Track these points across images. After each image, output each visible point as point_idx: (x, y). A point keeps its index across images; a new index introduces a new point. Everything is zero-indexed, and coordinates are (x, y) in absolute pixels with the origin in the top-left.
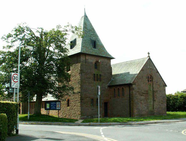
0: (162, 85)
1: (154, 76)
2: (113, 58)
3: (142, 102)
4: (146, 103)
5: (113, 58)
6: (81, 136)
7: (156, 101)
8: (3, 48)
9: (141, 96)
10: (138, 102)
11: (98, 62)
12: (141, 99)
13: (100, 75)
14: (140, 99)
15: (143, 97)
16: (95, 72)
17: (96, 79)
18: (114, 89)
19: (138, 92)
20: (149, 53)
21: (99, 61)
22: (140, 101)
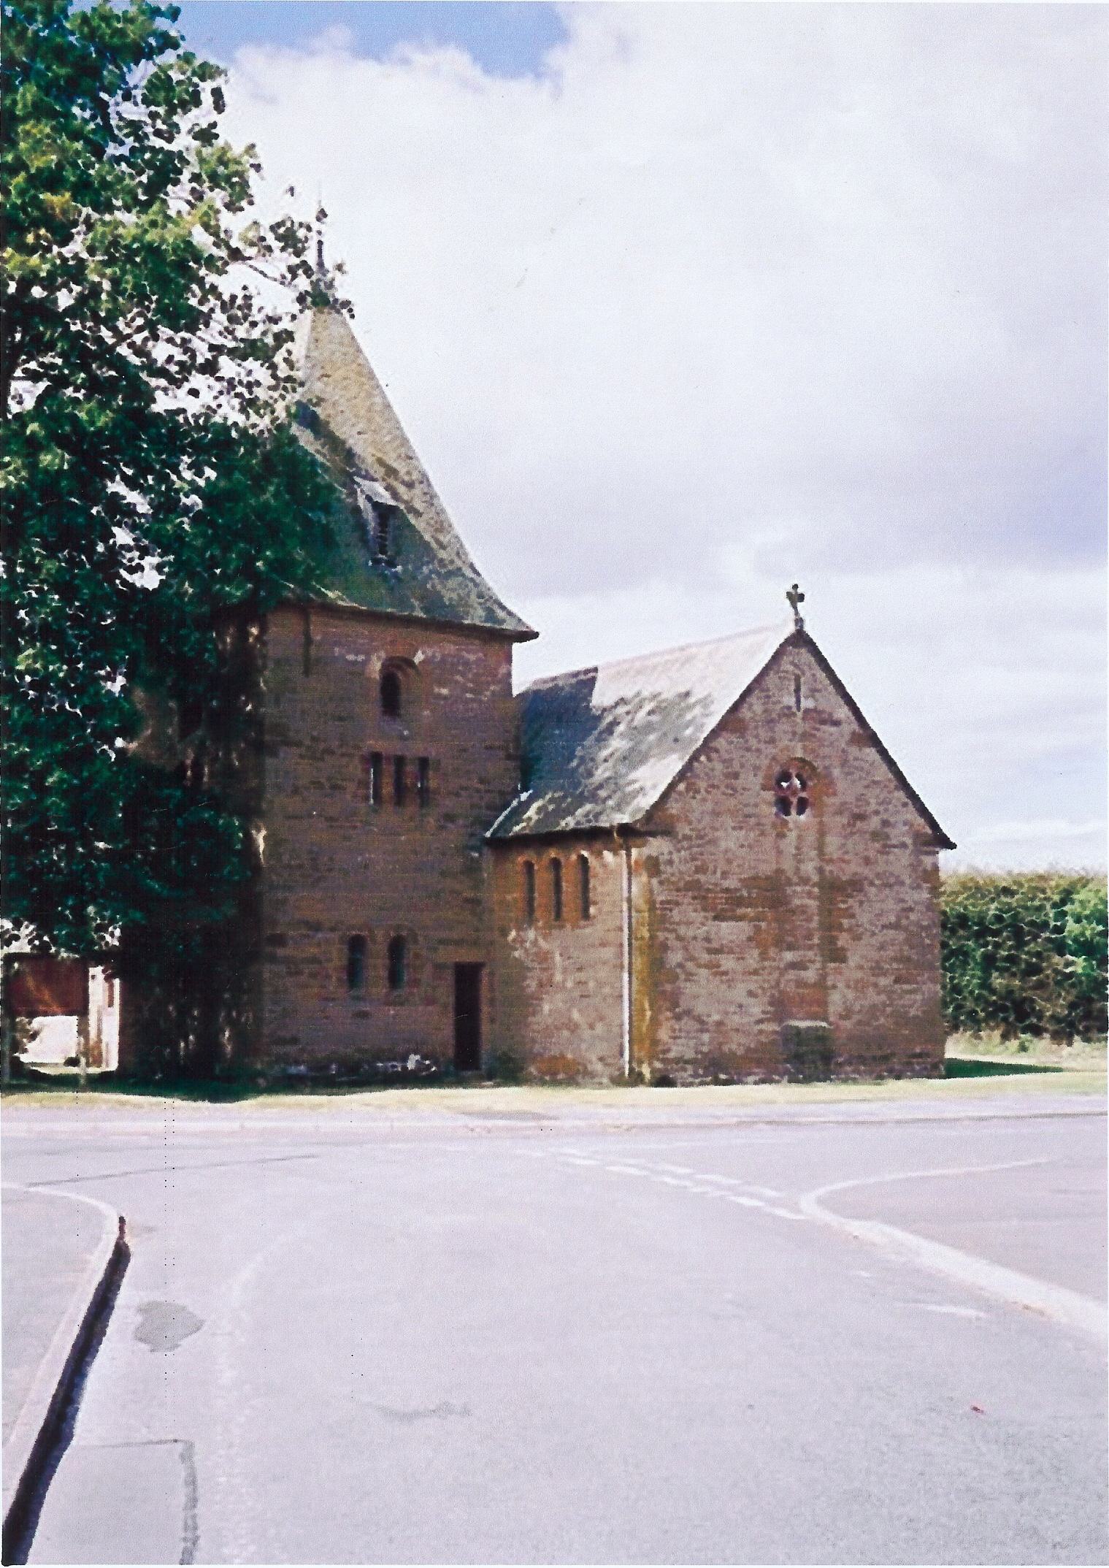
0: (904, 823)
1: (836, 772)
2: (529, 635)
3: (728, 963)
4: (755, 972)
5: (529, 635)
6: (998, 1065)
7: (853, 960)
8: (253, 146)
9: (715, 918)
10: (690, 965)
11: (410, 663)
12: (715, 945)
13: (424, 763)
14: (708, 940)
15: (729, 931)
16: (382, 738)
17: (388, 789)
18: (529, 866)
19: (693, 886)
20: (796, 597)
21: (419, 658)
22: (705, 957)
